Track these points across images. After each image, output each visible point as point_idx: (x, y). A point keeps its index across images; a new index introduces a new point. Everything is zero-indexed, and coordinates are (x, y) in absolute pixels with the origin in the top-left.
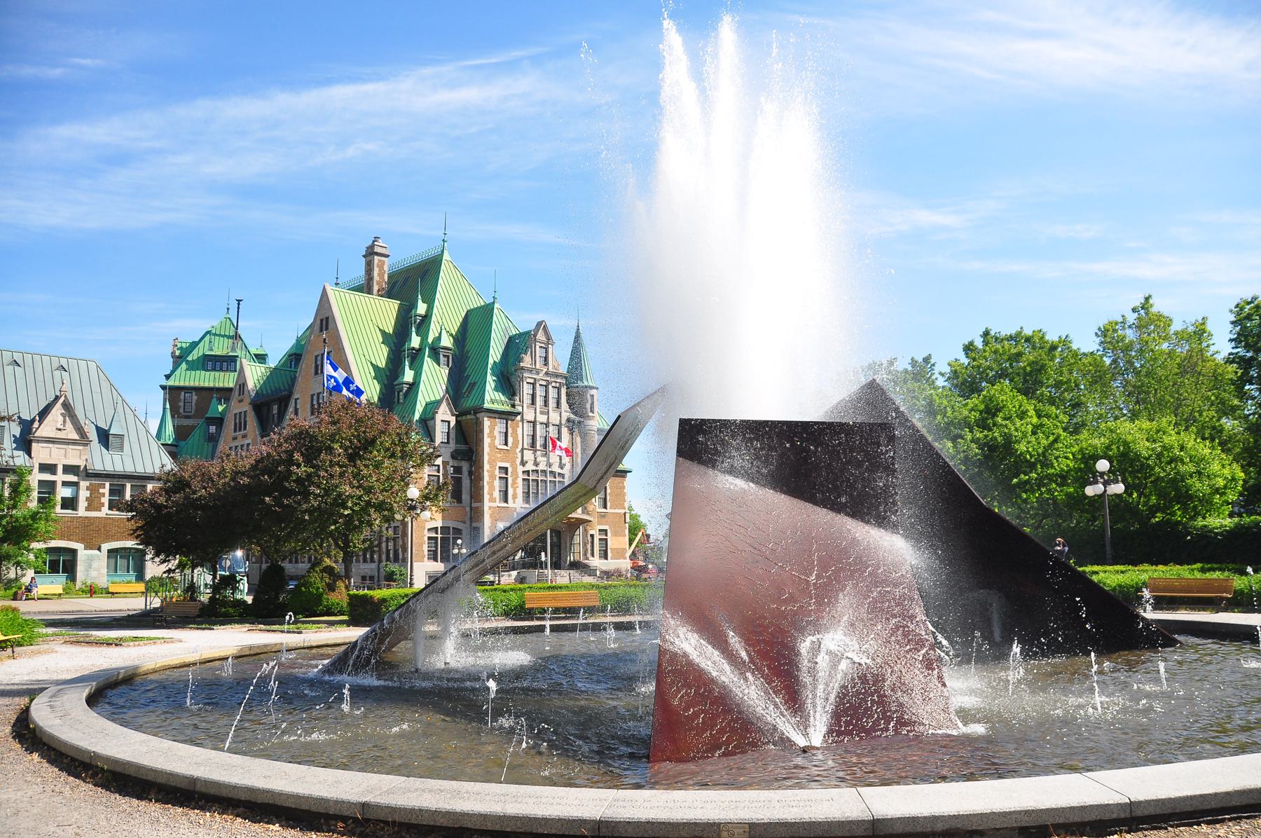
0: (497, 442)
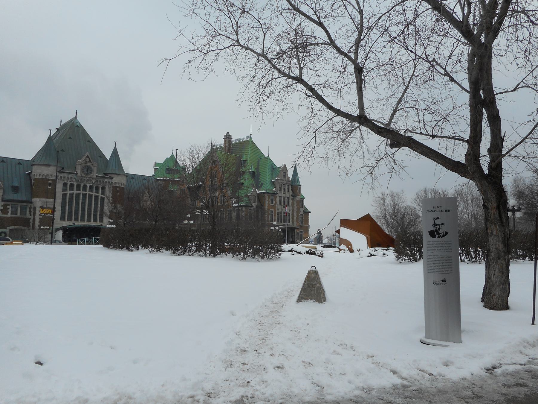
0: (270, 203)
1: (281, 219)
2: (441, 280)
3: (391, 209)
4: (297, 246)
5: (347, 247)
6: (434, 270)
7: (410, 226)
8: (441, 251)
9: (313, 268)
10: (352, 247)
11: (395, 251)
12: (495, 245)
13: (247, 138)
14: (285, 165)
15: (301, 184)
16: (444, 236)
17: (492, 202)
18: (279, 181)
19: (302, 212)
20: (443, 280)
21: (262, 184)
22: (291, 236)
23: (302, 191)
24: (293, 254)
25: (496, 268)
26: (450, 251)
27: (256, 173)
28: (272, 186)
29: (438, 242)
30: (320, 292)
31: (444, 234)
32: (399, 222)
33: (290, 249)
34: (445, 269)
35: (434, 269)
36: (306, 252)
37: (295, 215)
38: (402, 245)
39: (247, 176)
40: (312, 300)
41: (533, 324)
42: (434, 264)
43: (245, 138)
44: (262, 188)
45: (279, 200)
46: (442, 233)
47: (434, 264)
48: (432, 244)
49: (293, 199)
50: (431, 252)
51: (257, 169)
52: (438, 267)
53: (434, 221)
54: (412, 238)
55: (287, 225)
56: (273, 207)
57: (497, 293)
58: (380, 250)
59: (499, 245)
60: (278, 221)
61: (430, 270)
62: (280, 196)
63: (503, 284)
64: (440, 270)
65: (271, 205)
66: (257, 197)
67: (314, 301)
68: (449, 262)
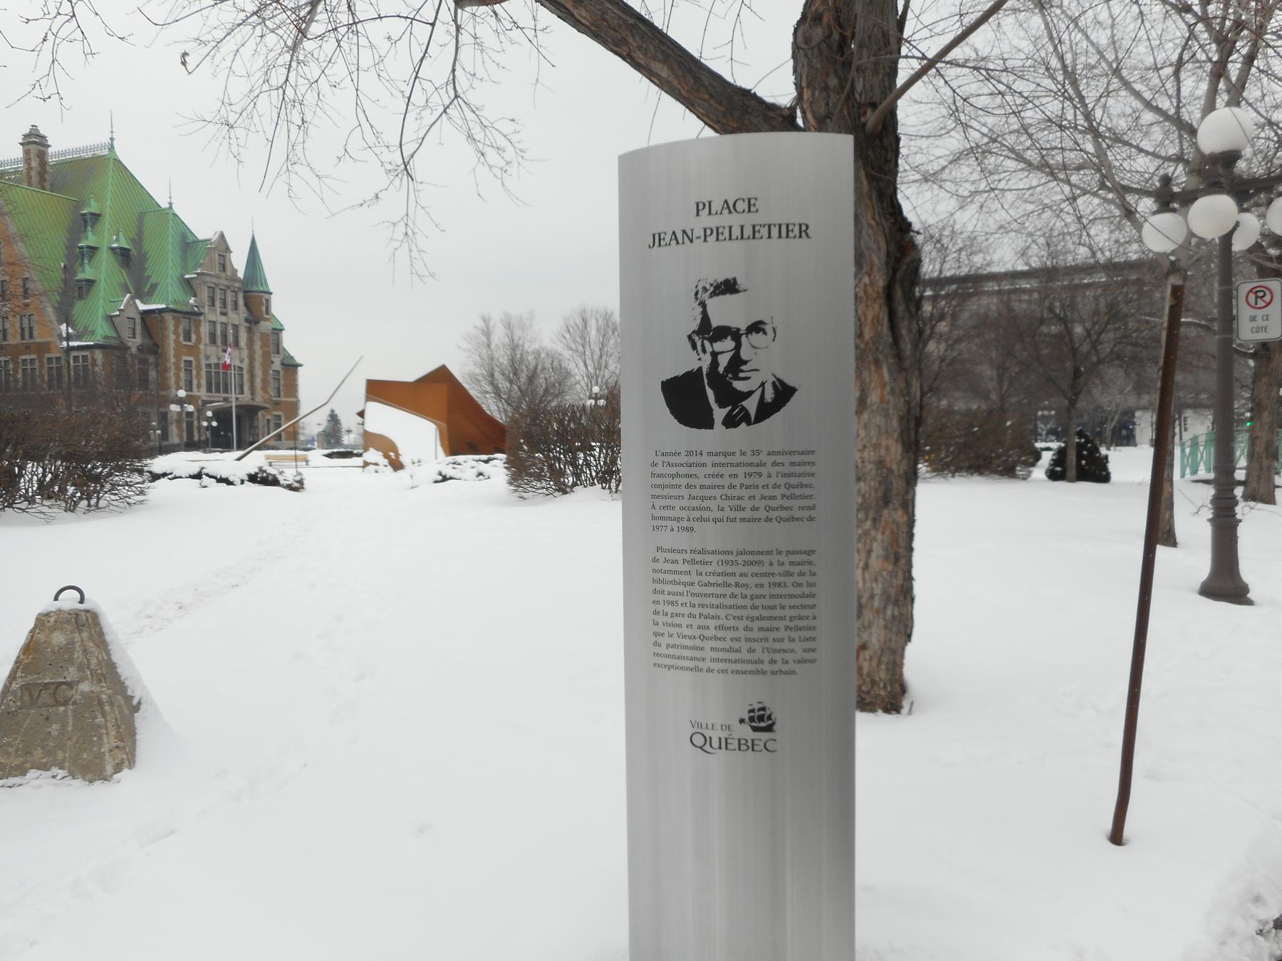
0: (181, 339)
1: (218, 384)
2: (742, 721)
3: (506, 358)
4: (239, 459)
5: (386, 456)
6: (698, 654)
7: (550, 398)
8: (742, 520)
9: (69, 601)
10: (397, 455)
11: (510, 464)
12: (874, 451)
13: (101, 147)
14: (222, 236)
15: (272, 291)
16: (765, 411)
17: (871, 270)
18: (208, 279)
19: (277, 366)
20: (752, 719)
21: (154, 287)
22: (248, 427)
23: (276, 309)
24: (203, 484)
25: (875, 539)
26: (806, 514)
27: (134, 252)
28: (185, 292)
29: (730, 459)
30: (100, 720)
31: (769, 396)
32: (523, 388)
33: (195, 471)
34: (767, 640)
35: (698, 643)
36: (246, 478)
37: (259, 372)
38: (525, 447)
39: (104, 257)
40: (49, 773)
41: (1117, 837)
42: (696, 611)
43: (92, 148)
44: (154, 297)
45: (207, 331)
46: (750, 393)
47: (696, 611)
48: (683, 470)
49: (250, 330)
50: (675, 524)
51: (138, 240)
52: (721, 627)
53: (703, 305)
54: (552, 426)
55: (234, 399)
56: (193, 350)
57: (874, 640)
58: (469, 462)
59: (887, 449)
60: (209, 390)
61: (672, 651)
62: (211, 319)
63: (896, 603)
64: (738, 651)
65: (185, 345)
66: (138, 321)
67: (61, 773)
68: (798, 591)
